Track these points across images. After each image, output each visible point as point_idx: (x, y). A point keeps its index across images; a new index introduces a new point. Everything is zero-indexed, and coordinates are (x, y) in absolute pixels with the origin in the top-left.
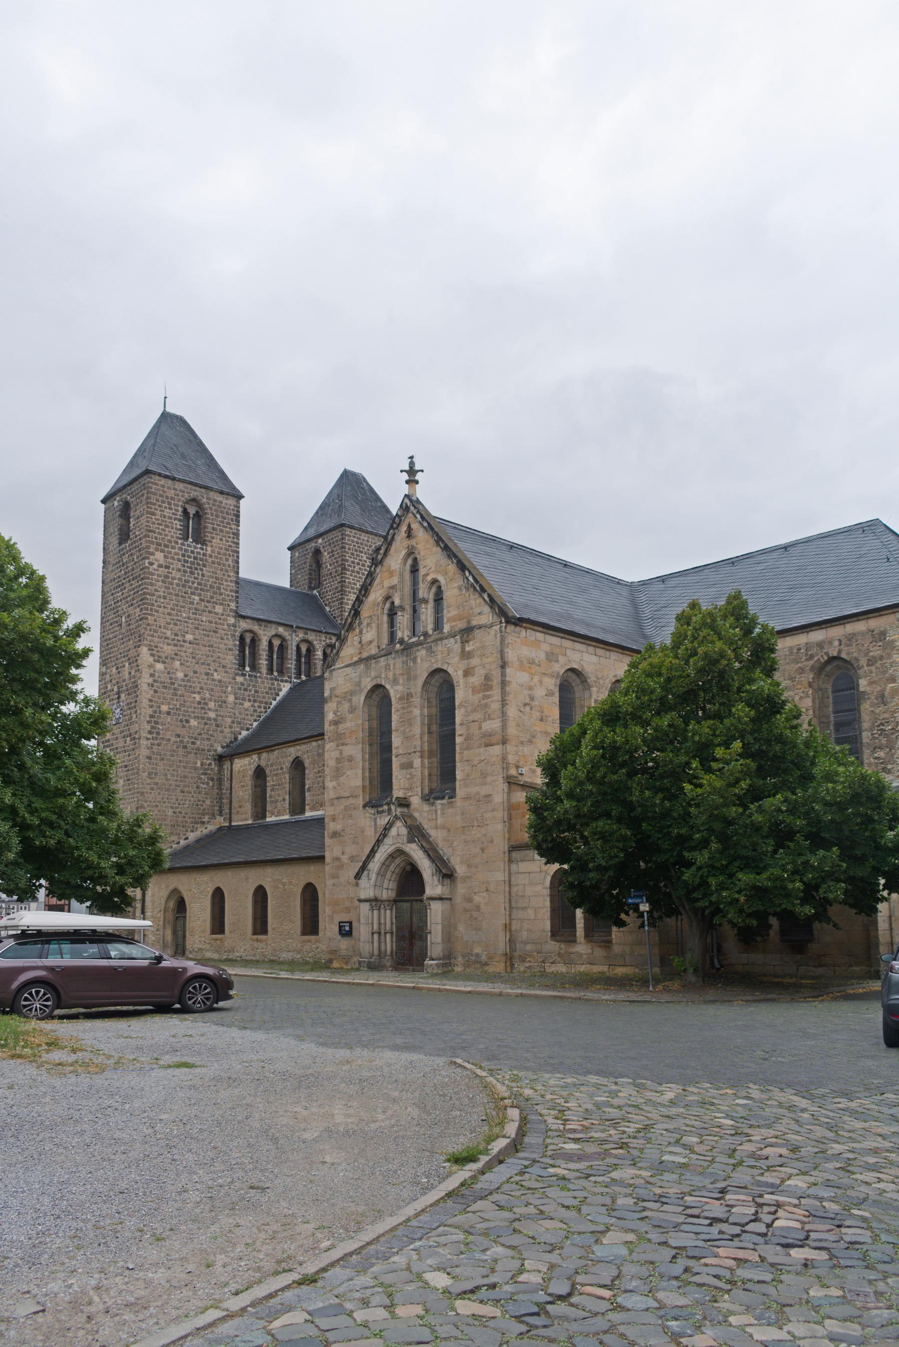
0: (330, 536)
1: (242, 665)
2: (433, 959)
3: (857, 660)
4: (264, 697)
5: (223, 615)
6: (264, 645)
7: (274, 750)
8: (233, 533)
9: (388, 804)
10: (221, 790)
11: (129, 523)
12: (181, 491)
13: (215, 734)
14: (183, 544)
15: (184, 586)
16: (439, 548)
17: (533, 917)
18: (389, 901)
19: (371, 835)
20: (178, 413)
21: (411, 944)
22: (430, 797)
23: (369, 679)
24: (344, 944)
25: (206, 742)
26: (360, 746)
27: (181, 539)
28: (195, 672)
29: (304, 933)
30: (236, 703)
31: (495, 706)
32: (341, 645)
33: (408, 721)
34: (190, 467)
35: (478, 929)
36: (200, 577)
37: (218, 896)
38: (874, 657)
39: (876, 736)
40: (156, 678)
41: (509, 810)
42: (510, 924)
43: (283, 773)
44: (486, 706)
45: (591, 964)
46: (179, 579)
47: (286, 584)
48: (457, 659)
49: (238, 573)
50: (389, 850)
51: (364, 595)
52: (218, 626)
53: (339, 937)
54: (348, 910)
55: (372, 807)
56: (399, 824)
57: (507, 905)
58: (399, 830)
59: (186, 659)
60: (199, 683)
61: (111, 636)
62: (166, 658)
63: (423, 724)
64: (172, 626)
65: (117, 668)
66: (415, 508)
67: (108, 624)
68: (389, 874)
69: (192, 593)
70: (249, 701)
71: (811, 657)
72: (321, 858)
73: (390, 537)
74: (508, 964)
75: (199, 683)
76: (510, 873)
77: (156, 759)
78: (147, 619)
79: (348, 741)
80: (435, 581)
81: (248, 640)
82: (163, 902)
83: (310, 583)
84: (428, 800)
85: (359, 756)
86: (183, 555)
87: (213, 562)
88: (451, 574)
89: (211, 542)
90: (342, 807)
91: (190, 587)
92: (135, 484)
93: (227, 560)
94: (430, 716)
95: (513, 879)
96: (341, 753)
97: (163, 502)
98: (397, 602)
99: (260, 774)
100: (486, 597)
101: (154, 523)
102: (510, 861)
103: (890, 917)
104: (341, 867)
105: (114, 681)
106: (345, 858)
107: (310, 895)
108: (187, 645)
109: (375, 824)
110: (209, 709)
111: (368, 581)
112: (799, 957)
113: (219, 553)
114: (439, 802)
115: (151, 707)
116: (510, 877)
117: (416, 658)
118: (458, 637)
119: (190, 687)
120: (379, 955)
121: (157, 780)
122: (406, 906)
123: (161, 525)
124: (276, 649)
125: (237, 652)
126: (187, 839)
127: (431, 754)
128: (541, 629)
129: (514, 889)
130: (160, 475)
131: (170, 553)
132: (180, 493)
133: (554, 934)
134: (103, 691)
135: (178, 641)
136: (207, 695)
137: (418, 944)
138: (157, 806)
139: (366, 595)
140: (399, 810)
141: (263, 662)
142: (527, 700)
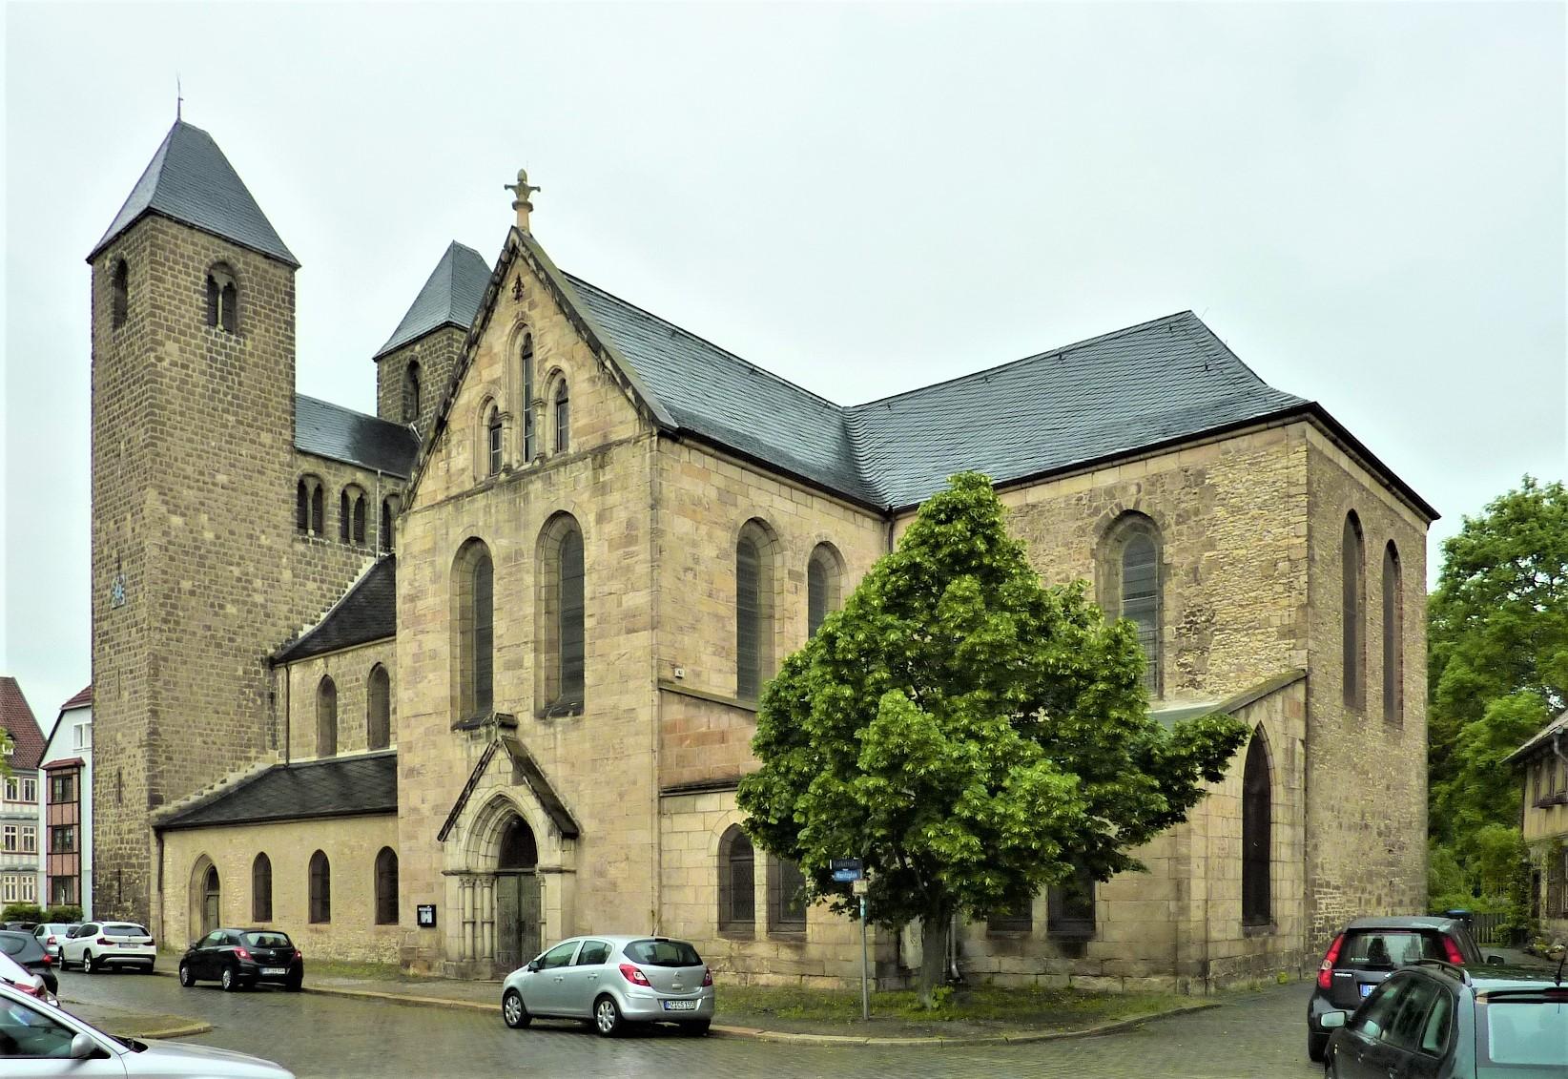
0: (431, 340)
1: (302, 526)
3: (1162, 515)
6: (333, 499)
8: (286, 322)
12: (203, 247)
13: (265, 628)
15: (212, 399)
16: (561, 318)
17: (430, 921)
18: (487, 874)
20: (200, 126)
21: (520, 940)
22: (550, 712)
24: (426, 938)
25: (252, 640)
27: (205, 324)
28: (232, 533)
29: (380, 921)
31: (642, 569)
39: (1184, 631)
40: (172, 538)
41: (660, 732)
42: (659, 910)
43: (359, 687)
44: (629, 569)
46: (203, 386)
48: (586, 496)
49: (293, 384)
51: (453, 395)
52: (265, 464)
53: (418, 928)
54: (430, 888)
57: (656, 881)
58: (502, 762)
59: (217, 511)
60: (239, 549)
61: (106, 472)
62: (187, 508)
63: (538, 599)
65: (116, 522)
67: (101, 453)
68: (487, 832)
69: (227, 411)
70: (315, 580)
71: (1097, 510)
72: (392, 811)
75: (239, 549)
76: (660, 833)
78: (154, 445)
79: (430, 627)
80: (557, 371)
81: (311, 490)
82: (188, 873)
83: (405, 412)
85: (445, 650)
86: (210, 350)
87: (256, 365)
88: (579, 358)
89: (252, 332)
90: (422, 729)
91: (221, 401)
92: (133, 231)
93: (277, 363)
94: (548, 587)
95: (664, 842)
97: (176, 262)
99: (327, 687)
100: (630, 394)
101: (162, 295)
104: (421, 821)
105: (112, 542)
106: (426, 809)
107: (387, 863)
108: (220, 490)
109: (469, 756)
110: (255, 591)
112: (1072, 963)
114: (559, 720)
117: (527, 494)
118: (589, 460)
119: (225, 554)
120: (474, 957)
121: (177, 694)
122: (512, 881)
124: (352, 506)
125: (296, 507)
126: (224, 782)
127: (550, 646)
129: (666, 857)
131: (189, 345)
132: (198, 254)
134: (97, 557)
136: (251, 569)
140: (501, 733)
141: (333, 522)
142: (690, 563)
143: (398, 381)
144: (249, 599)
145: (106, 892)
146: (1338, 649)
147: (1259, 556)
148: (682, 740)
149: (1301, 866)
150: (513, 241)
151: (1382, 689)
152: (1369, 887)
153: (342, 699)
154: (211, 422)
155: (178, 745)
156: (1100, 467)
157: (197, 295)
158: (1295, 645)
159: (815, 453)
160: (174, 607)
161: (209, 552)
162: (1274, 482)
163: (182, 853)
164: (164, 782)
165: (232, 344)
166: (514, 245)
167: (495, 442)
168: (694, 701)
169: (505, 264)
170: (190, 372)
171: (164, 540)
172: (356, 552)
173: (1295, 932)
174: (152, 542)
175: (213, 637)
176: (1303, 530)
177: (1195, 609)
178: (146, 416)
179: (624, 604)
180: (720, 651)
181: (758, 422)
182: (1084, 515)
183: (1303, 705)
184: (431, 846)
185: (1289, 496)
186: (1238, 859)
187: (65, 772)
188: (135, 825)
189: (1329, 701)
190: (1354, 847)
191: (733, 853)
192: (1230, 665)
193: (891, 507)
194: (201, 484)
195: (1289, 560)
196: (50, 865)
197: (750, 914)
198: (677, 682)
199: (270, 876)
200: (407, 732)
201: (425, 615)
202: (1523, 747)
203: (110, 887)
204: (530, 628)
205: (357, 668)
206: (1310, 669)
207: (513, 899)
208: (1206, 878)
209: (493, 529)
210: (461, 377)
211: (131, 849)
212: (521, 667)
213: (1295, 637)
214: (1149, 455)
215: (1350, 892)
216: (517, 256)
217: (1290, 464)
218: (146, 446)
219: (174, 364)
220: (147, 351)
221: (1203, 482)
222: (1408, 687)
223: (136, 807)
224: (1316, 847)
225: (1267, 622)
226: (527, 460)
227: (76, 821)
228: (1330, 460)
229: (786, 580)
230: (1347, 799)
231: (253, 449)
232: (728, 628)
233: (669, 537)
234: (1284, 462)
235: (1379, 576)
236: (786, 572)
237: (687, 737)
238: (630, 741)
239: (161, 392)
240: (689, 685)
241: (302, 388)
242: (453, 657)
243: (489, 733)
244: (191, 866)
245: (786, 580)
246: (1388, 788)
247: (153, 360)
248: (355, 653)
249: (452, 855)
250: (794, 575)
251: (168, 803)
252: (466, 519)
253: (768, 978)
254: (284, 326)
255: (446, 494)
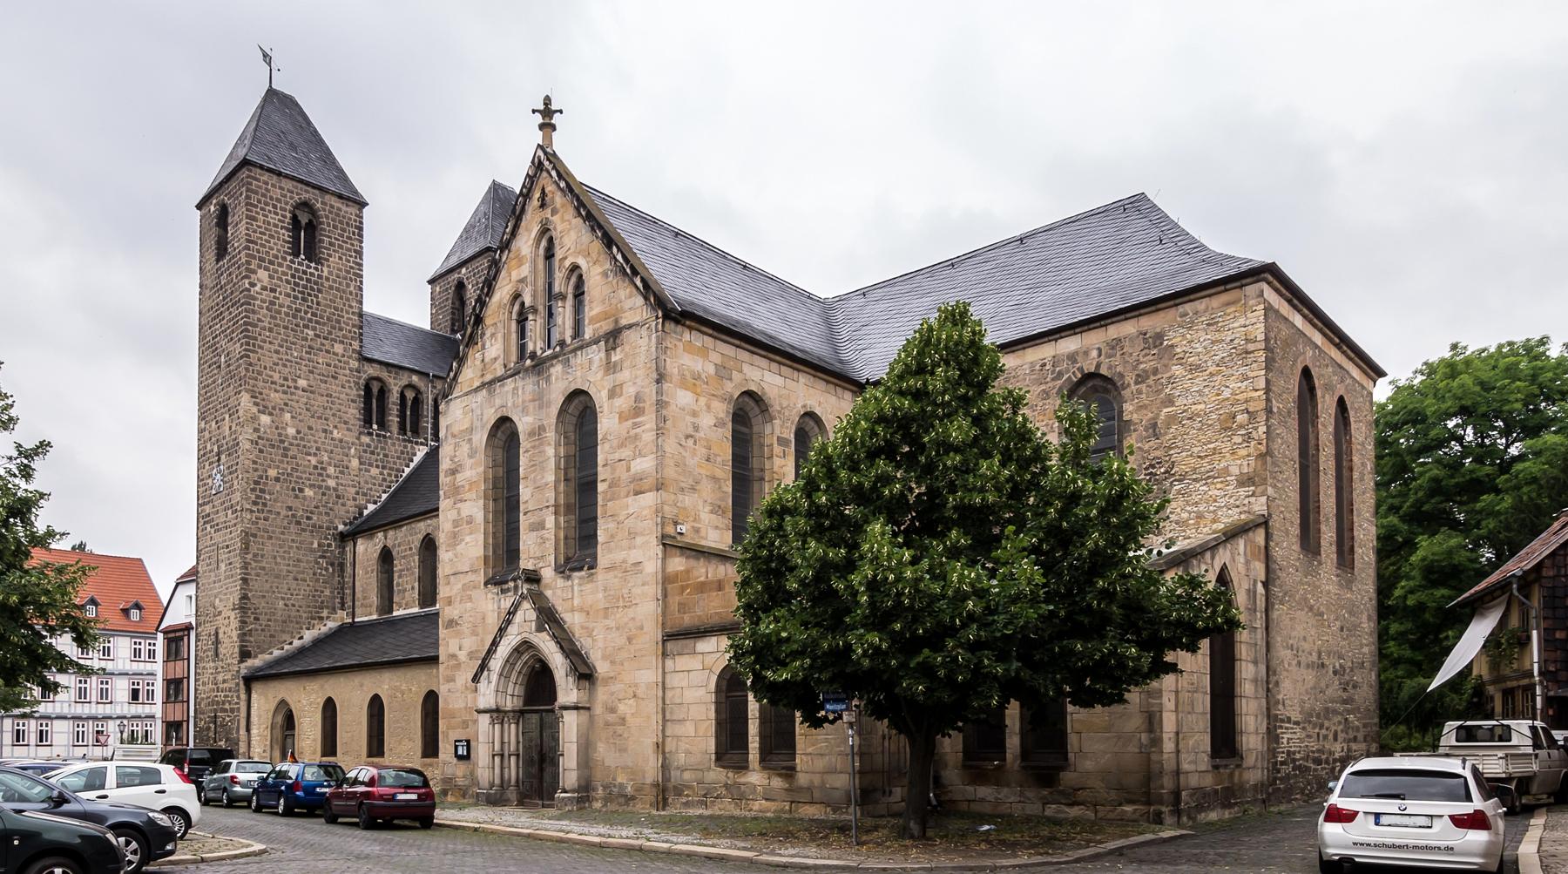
0: (475, 264)
1: (368, 422)
2: (566, 792)
3: (1121, 376)
4: (395, 463)
5: (343, 356)
6: (394, 397)
7: (402, 526)
8: (355, 251)
9: (514, 580)
10: (343, 578)
11: (227, 232)
12: (289, 191)
13: (336, 507)
14: (292, 262)
15: (295, 317)
16: (579, 220)
18: (513, 711)
19: (493, 623)
21: (541, 770)
23: (493, 411)
26: (482, 501)
30: (360, 470)
31: (648, 437)
32: (459, 366)
33: (536, 466)
34: (300, 161)
35: (623, 750)
36: (315, 306)
37: (330, 708)
38: (1144, 371)
40: (261, 434)
41: (663, 583)
42: (663, 742)
43: (412, 555)
44: (636, 437)
45: (767, 800)
46: (288, 307)
47: (428, 327)
49: (361, 303)
50: (514, 643)
51: (487, 295)
54: (465, 724)
55: (495, 584)
56: (526, 605)
57: (660, 716)
58: (527, 613)
60: (316, 442)
62: (274, 408)
63: (558, 467)
64: (280, 367)
65: (217, 423)
66: (551, 162)
67: (206, 366)
69: (306, 326)
70: (377, 466)
71: (1060, 374)
72: (434, 660)
73: (518, 208)
74: (660, 797)
75: (316, 442)
76: (664, 673)
77: (263, 537)
78: (248, 356)
81: (375, 390)
82: (271, 714)
83: (453, 325)
84: (563, 572)
85: (479, 516)
86: (293, 276)
88: (594, 255)
89: (328, 261)
90: (460, 586)
91: (302, 318)
92: (233, 180)
93: (348, 286)
94: (567, 457)
96: (459, 513)
98: (528, 302)
99: (386, 557)
101: (255, 232)
102: (665, 655)
103: (1177, 734)
104: (458, 666)
106: (462, 655)
108: (300, 392)
110: (328, 476)
111: (492, 273)
113: (338, 277)
114: (576, 574)
115: (256, 470)
116: (664, 678)
119: (304, 446)
120: (502, 785)
121: (264, 565)
122: (535, 718)
123: (265, 234)
124: (409, 403)
126: (301, 638)
127: (569, 509)
128: (710, 331)
129: (669, 694)
130: (261, 167)
131: (276, 272)
132: (285, 195)
133: (720, 757)
134: (202, 452)
135: (288, 387)
136: (326, 458)
137: (548, 770)
138: (264, 597)
139: (489, 294)
140: (526, 586)
141: (393, 419)
142: (690, 431)
143: (447, 299)
144: (324, 484)
145: (205, 733)
146: (1294, 497)
147: (1217, 409)
148: (683, 589)
149: (1264, 701)
150: (539, 157)
151: (1334, 535)
152: (1327, 724)
153: (398, 565)
154: (295, 336)
155: (264, 608)
156: (1063, 334)
157: (283, 231)
158: (1254, 492)
159: (801, 335)
160: (262, 491)
161: (291, 444)
162: (1232, 341)
163: (263, 702)
164: (252, 639)
165: (312, 270)
166: (540, 160)
167: (522, 333)
168: (694, 553)
169: (531, 180)
170: (277, 295)
171: (255, 435)
172: (411, 442)
173: (1259, 765)
174: (246, 436)
175: (293, 516)
176: (1262, 384)
177: (1154, 462)
178: (241, 333)
179: (633, 470)
180: (717, 510)
181: (750, 310)
182: (1048, 379)
183: (1263, 548)
184: (467, 688)
185: (1247, 353)
186: (1206, 693)
187: (177, 634)
188: (228, 676)
189: (1287, 547)
190: (1311, 684)
191: (729, 689)
192: (1190, 513)
193: (868, 379)
194: (285, 388)
195: (1248, 412)
196: (165, 712)
197: (744, 746)
198: (679, 538)
199: (383, 735)
200: (448, 588)
201: (463, 486)
202: (1472, 591)
203: (208, 729)
204: (551, 495)
205: (410, 538)
206: (1270, 515)
207: (535, 734)
208: (1176, 710)
209: (520, 408)
210: (494, 279)
211: (226, 696)
212: (543, 528)
213: (1253, 484)
214: (1109, 321)
215: (1309, 728)
216: (542, 170)
217: (1247, 323)
218: (241, 358)
219: (263, 288)
220: (242, 279)
221: (1162, 344)
222: (1359, 534)
223: (229, 661)
224: (1277, 684)
225: (1226, 471)
226: (549, 347)
227: (186, 675)
228: (1286, 319)
229: (775, 445)
230: (1305, 639)
231: (328, 358)
232: (725, 489)
233: (672, 407)
234: (1242, 321)
235: (1331, 429)
236: (775, 438)
237: (688, 586)
238: (637, 591)
239: (254, 312)
240: (689, 539)
241: (367, 308)
242: (486, 521)
243: (516, 587)
244: (273, 709)
245: (775, 445)
246: (1342, 629)
247: (247, 286)
248: (409, 527)
249: (484, 695)
250: (783, 442)
251: (256, 657)
252: (498, 402)
253: (760, 805)
254: (354, 254)
255: (481, 380)
